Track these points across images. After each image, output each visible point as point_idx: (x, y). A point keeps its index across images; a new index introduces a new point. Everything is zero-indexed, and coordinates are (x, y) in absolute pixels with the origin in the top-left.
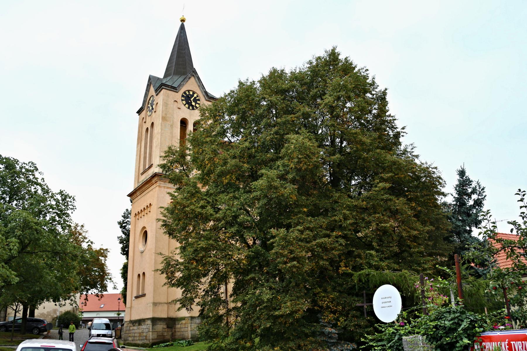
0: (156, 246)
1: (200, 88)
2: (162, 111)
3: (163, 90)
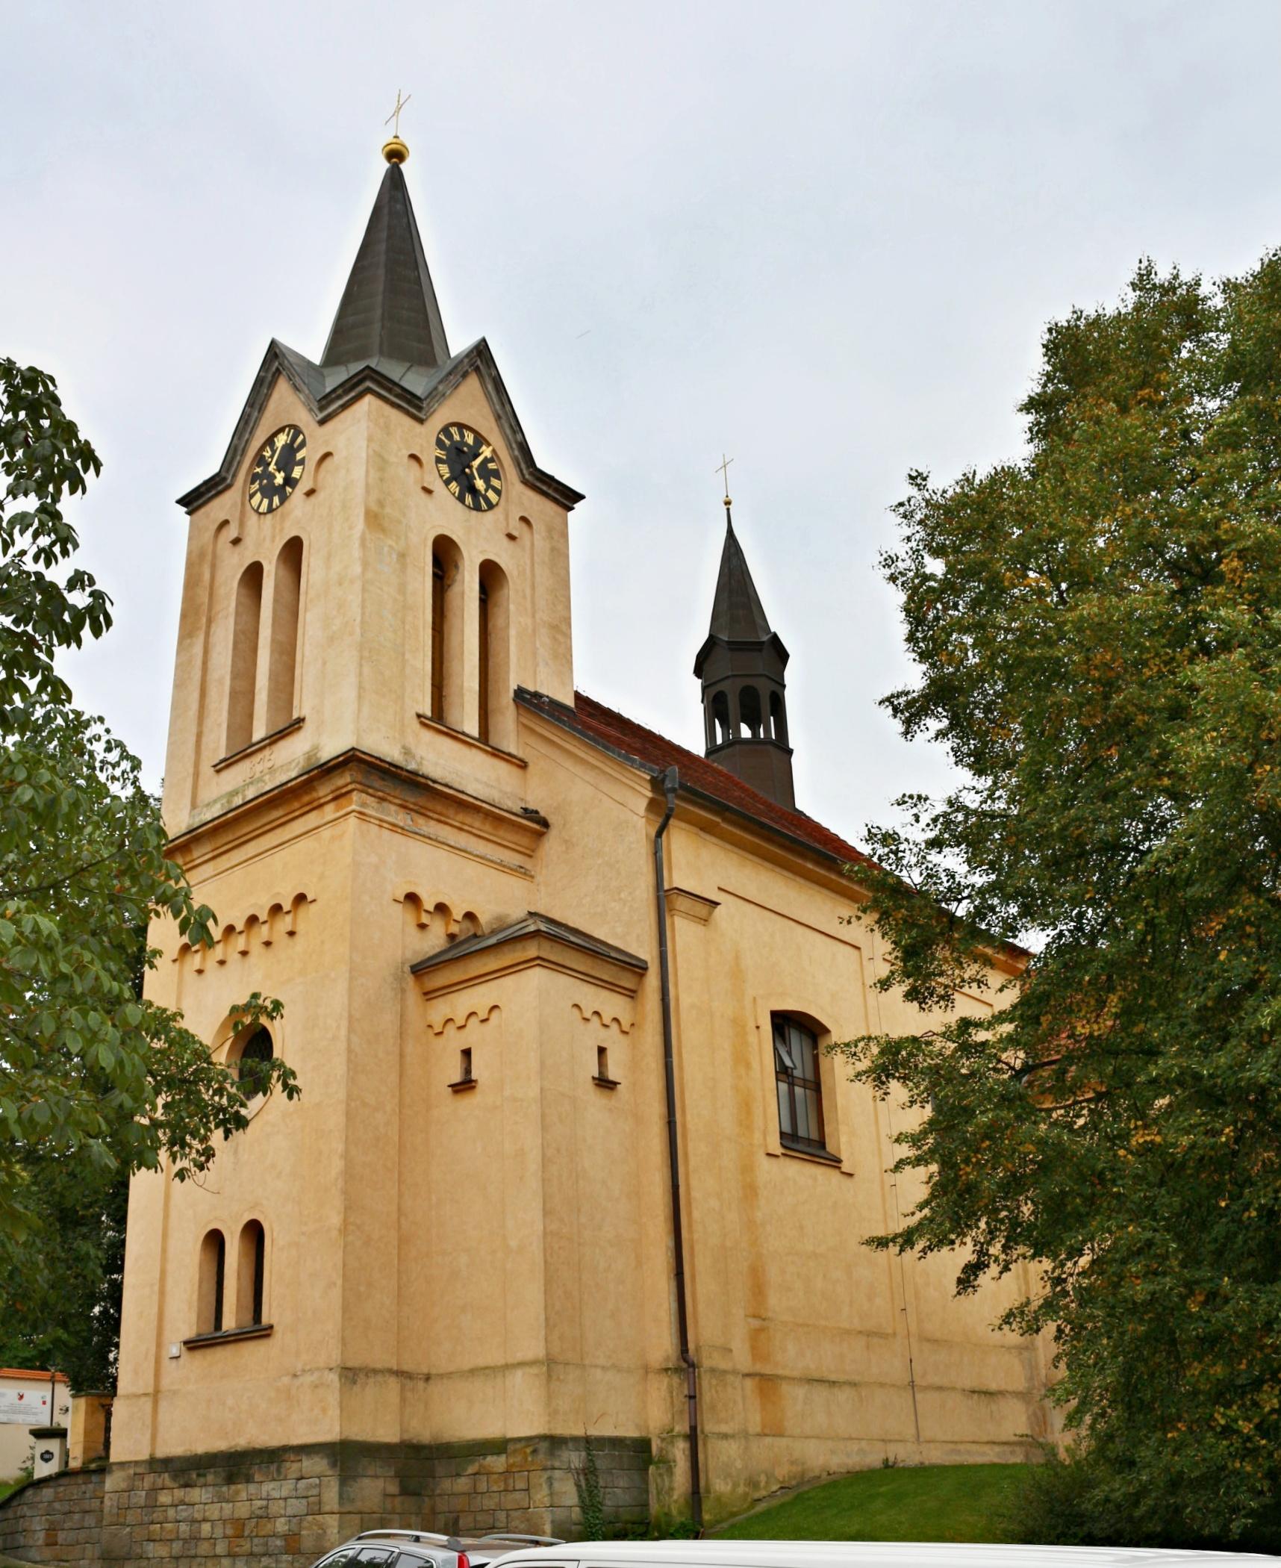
0: (350, 1097)
1: (501, 427)
2: (367, 485)
3: (368, 399)
